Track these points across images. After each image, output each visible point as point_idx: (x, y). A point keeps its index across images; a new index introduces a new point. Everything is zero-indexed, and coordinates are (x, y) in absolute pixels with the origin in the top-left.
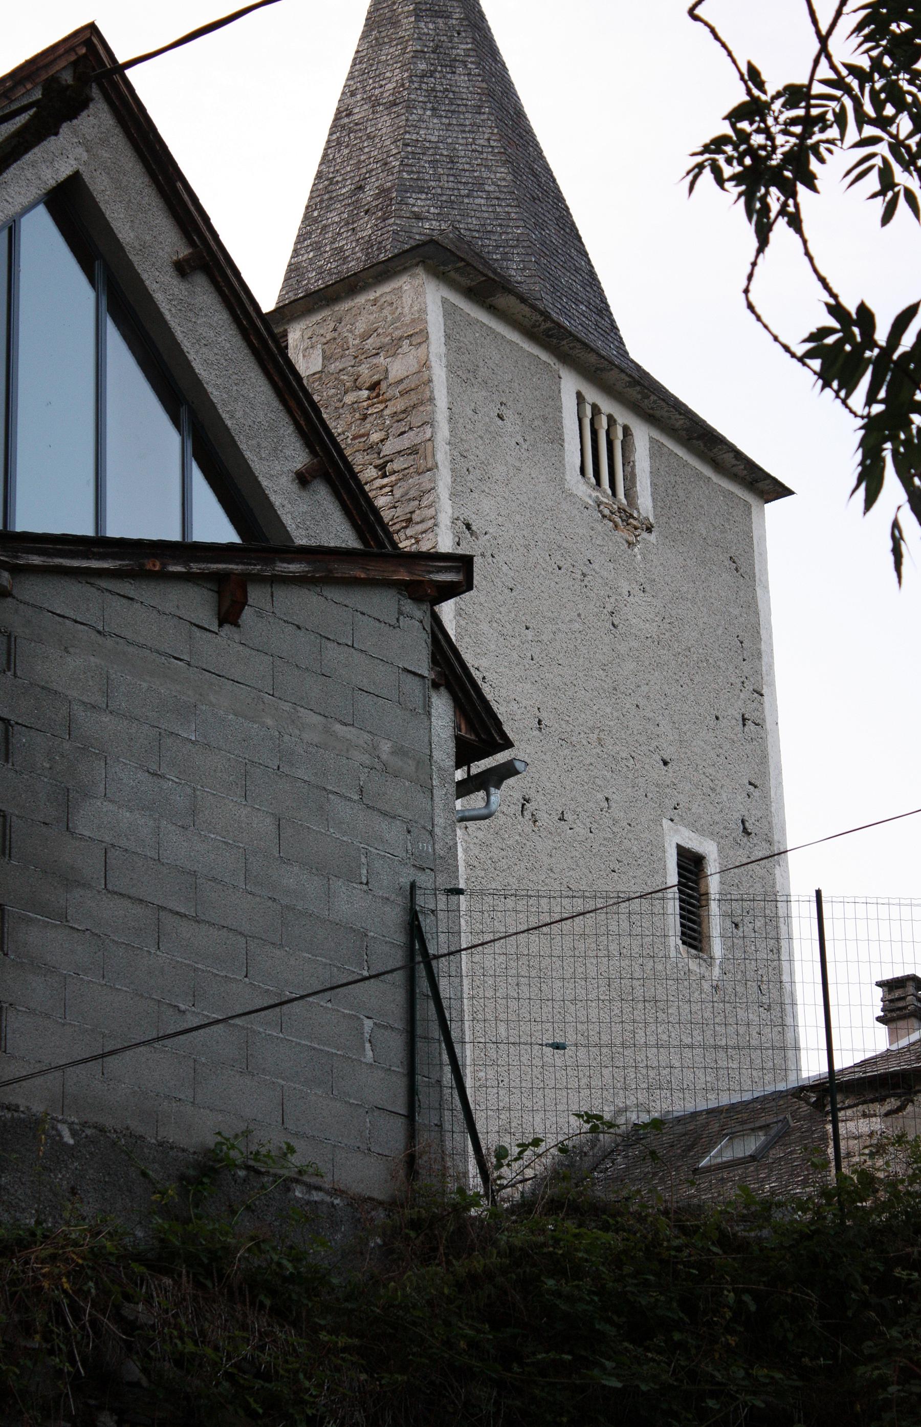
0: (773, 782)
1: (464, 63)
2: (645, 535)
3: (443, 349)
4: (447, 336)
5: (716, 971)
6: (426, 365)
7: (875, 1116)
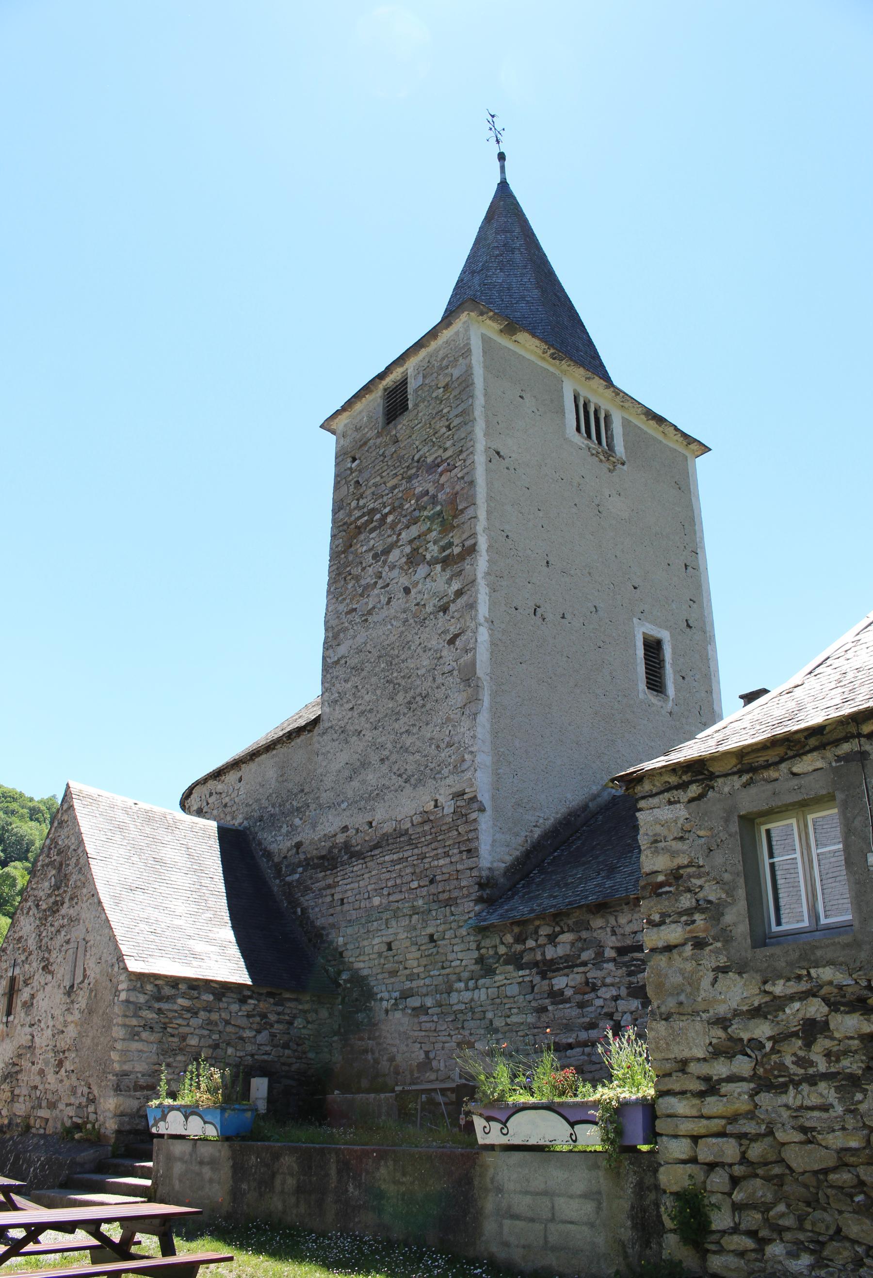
0: (705, 600)
1: (519, 249)
2: (620, 466)
3: (481, 359)
4: (484, 352)
5: (670, 704)
6: (470, 367)
7: (679, 802)
